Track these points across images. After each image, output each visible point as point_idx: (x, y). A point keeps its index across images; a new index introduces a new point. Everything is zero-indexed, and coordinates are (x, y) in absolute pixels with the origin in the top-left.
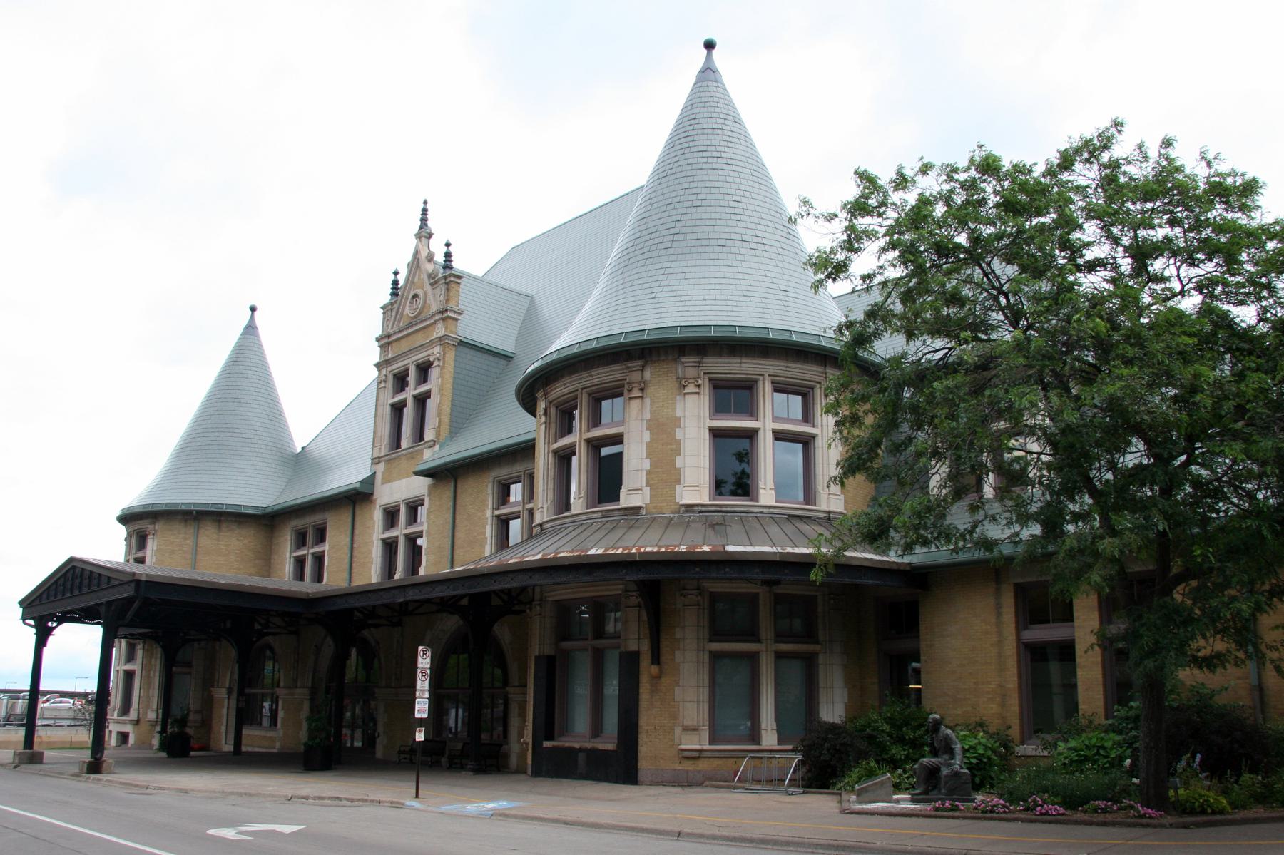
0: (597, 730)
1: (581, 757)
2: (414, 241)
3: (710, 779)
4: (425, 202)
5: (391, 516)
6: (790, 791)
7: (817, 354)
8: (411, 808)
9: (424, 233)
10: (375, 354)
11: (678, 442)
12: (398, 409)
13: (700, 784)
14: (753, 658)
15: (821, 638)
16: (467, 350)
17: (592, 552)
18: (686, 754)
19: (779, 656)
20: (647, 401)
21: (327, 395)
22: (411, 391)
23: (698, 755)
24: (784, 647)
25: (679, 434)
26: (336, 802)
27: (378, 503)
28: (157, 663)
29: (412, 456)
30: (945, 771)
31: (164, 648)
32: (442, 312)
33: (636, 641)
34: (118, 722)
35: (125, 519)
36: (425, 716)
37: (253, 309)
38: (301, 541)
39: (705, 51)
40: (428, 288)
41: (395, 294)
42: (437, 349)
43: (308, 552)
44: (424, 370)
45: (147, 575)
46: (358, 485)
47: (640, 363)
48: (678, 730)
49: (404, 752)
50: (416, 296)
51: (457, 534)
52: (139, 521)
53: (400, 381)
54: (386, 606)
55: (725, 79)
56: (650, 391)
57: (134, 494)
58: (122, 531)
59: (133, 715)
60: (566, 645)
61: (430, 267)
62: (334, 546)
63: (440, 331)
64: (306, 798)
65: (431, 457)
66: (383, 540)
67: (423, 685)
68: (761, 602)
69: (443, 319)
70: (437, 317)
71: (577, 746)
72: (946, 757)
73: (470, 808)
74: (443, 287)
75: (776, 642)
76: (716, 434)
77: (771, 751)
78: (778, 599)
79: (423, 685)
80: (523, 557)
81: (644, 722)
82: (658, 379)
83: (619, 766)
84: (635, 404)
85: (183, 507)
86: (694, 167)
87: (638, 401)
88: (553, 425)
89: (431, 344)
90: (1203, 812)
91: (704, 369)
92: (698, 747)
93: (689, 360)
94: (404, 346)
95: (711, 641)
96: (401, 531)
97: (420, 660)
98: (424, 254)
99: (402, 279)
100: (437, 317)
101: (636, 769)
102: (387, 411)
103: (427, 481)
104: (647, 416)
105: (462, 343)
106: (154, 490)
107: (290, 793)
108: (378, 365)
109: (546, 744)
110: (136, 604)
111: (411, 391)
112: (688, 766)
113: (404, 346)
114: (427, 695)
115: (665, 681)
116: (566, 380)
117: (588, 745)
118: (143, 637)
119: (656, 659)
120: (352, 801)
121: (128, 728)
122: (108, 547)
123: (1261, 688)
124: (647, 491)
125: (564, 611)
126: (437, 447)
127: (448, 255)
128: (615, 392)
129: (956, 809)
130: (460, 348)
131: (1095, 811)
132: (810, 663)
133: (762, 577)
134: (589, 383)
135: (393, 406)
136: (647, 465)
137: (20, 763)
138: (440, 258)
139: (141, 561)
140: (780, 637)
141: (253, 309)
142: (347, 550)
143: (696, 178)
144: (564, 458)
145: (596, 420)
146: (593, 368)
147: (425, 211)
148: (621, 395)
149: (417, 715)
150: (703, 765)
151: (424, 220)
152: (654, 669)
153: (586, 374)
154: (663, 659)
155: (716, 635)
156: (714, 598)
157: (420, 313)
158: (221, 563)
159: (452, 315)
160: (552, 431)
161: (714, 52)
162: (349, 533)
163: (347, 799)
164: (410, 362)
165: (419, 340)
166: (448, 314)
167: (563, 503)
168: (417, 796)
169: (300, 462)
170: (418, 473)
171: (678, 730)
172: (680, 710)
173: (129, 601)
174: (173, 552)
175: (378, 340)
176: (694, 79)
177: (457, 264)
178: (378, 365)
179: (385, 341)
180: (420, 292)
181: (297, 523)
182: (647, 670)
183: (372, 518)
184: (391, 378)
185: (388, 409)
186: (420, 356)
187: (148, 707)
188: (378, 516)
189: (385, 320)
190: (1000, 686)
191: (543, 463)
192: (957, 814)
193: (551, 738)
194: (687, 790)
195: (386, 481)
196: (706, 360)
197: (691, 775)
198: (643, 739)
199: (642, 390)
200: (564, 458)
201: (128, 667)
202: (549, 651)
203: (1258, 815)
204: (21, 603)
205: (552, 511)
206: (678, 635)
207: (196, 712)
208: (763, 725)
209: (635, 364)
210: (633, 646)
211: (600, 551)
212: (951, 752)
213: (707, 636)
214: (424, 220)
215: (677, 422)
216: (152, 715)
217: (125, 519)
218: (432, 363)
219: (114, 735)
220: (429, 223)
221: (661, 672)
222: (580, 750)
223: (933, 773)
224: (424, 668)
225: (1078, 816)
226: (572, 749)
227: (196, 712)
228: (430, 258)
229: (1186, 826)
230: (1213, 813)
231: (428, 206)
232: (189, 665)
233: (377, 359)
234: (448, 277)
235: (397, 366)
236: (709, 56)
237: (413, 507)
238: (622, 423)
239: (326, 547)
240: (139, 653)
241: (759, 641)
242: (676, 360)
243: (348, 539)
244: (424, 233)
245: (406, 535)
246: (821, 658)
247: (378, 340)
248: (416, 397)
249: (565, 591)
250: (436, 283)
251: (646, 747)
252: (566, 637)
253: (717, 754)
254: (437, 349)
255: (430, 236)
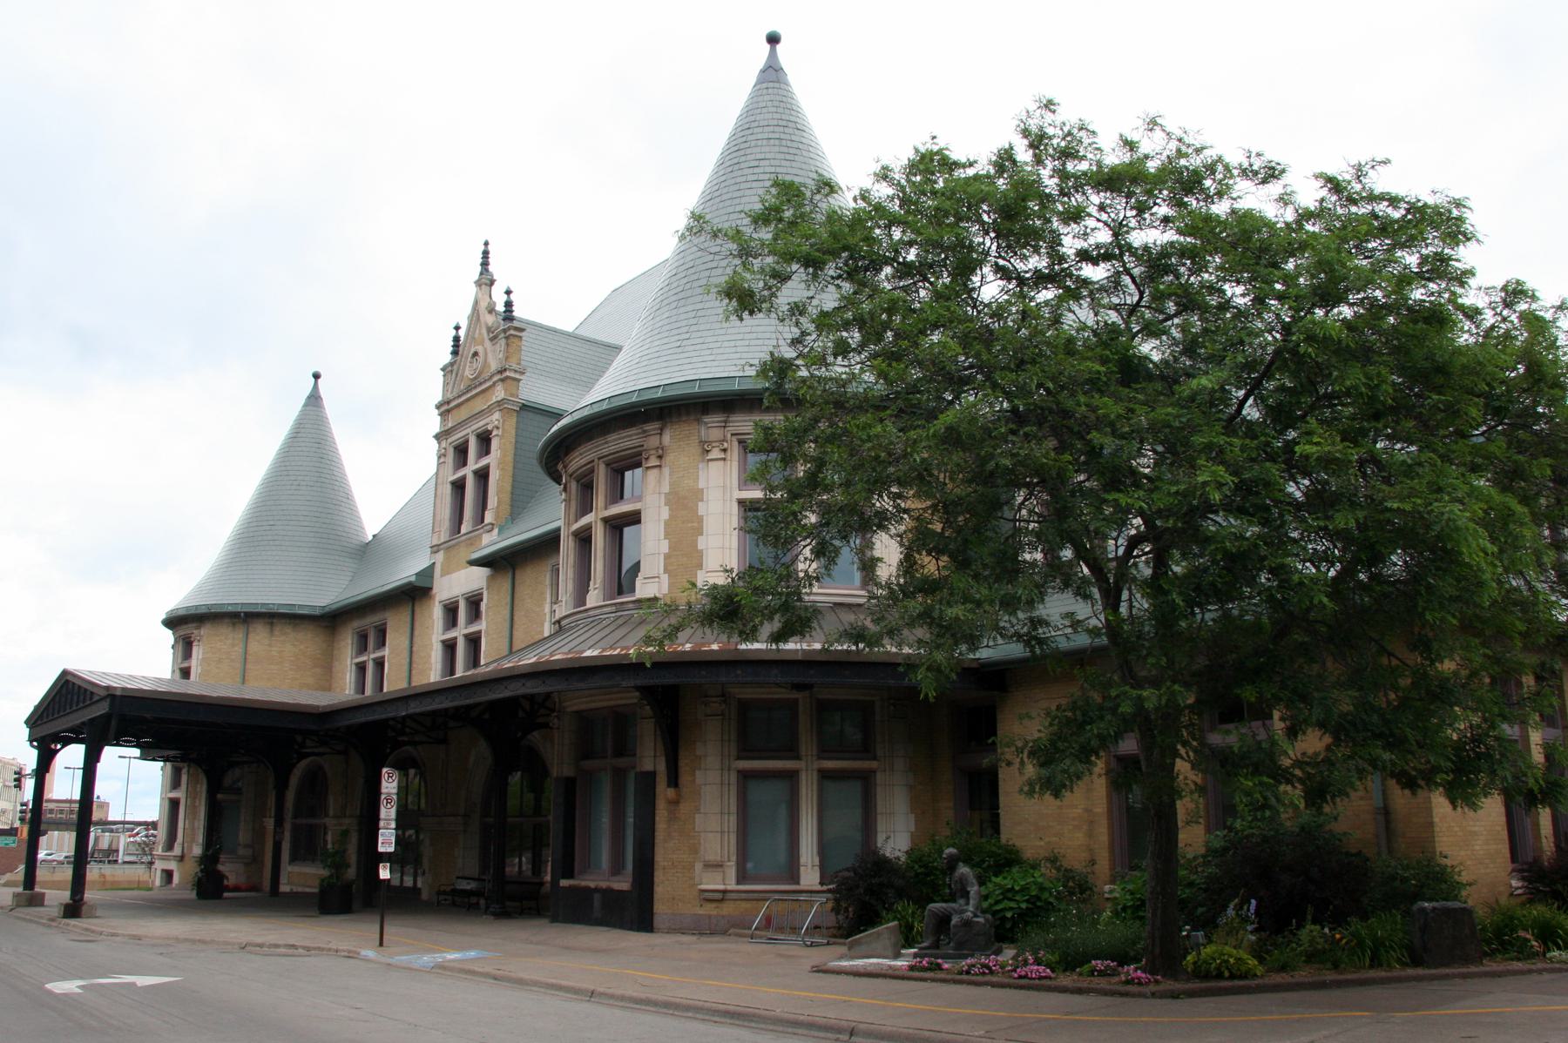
0: (617, 869)
1: (597, 897)
2: (473, 289)
3: (733, 926)
4: (486, 244)
5: (451, 611)
6: (808, 940)
7: (615, 419)
8: (367, 960)
9: (486, 280)
10: (434, 424)
11: (700, 520)
12: (459, 486)
13: (724, 933)
14: (792, 777)
15: (879, 753)
16: (531, 415)
17: (588, 653)
18: (710, 895)
19: (825, 775)
20: (666, 471)
21: (392, 476)
22: (473, 464)
23: (723, 896)
24: (829, 764)
25: (702, 509)
26: (291, 951)
27: (437, 599)
28: (203, 788)
29: (473, 541)
30: (955, 920)
31: (208, 774)
32: (500, 372)
33: (650, 758)
34: (163, 858)
35: (172, 622)
36: (391, 849)
37: (317, 376)
38: (362, 648)
39: (768, 47)
40: (488, 344)
41: (455, 353)
42: (497, 415)
43: (369, 658)
44: (485, 439)
45: (124, 689)
46: (413, 579)
47: (656, 425)
48: (699, 866)
49: (444, 893)
50: (476, 354)
51: (515, 633)
52: (184, 624)
53: (461, 452)
54: (393, 719)
55: (791, 78)
56: (669, 458)
57: (179, 592)
58: (168, 636)
59: (177, 851)
60: (588, 764)
61: (490, 319)
62: (393, 651)
63: (499, 393)
64: (261, 946)
65: (491, 542)
66: (443, 642)
67: (388, 813)
68: (801, 709)
69: (502, 380)
70: (496, 378)
71: (592, 885)
72: (962, 901)
73: (427, 959)
74: (503, 342)
75: (819, 758)
76: (741, 502)
77: (811, 892)
78: (823, 707)
79: (388, 813)
80: (551, 655)
81: (661, 857)
82: (675, 440)
83: (633, 911)
84: (653, 474)
85: (230, 609)
86: (743, 186)
87: (656, 471)
88: (573, 503)
89: (488, 411)
90: (1220, 976)
91: (731, 429)
92: (721, 887)
93: (714, 419)
94: (463, 413)
95: (739, 758)
96: (460, 632)
97: (384, 784)
98: (483, 305)
99: (462, 333)
100: (496, 378)
101: (652, 914)
102: (448, 489)
103: (483, 572)
104: (666, 489)
105: (526, 408)
106: (199, 589)
107: (244, 940)
108: (438, 437)
109: (564, 883)
110: (114, 723)
111: (473, 464)
112: (710, 909)
113: (463, 413)
114: (393, 825)
115: (684, 808)
116: (582, 449)
117: (604, 885)
118: (183, 759)
119: (674, 781)
120: (308, 949)
121: (172, 865)
122: (143, 660)
123: (1386, 812)
124: (665, 578)
125: (585, 722)
126: (496, 531)
127: (509, 304)
128: (634, 460)
129: (939, 967)
130: (524, 414)
131: (1092, 973)
132: (866, 780)
133: (632, 683)
134: (605, 452)
135: (454, 483)
136: (664, 547)
137: (18, 906)
138: (500, 308)
139: (186, 673)
140: (824, 752)
141: (317, 376)
142: (406, 654)
143: (744, 200)
144: (584, 539)
145: (617, 494)
146: (609, 432)
147: (486, 254)
148: (639, 465)
149: (381, 849)
150: (727, 909)
151: (485, 264)
152: (671, 792)
153: (601, 441)
154: (684, 779)
155: (746, 751)
156: (744, 707)
157: (480, 373)
158: (275, 676)
159: (512, 375)
160: (573, 509)
161: (778, 47)
162: (408, 630)
163: (304, 948)
164: (470, 433)
165: (479, 405)
166: (508, 373)
167: (580, 598)
168: (381, 944)
169: (367, 552)
170: (473, 563)
171: (699, 866)
172: (701, 839)
173: (106, 718)
174: (220, 661)
175: (438, 407)
176: (754, 81)
177: (518, 312)
178: (438, 437)
179: (445, 408)
180: (480, 349)
181: (357, 624)
182: (663, 792)
183: (431, 616)
184: (451, 451)
185: (449, 487)
186: (478, 425)
187: (193, 840)
188: (437, 613)
189: (446, 384)
190: (1087, 810)
191: (567, 547)
192: (940, 975)
193: (571, 875)
194: (704, 939)
195: (446, 571)
196: (733, 418)
197: (717, 922)
198: (659, 876)
199: (660, 457)
200: (584, 539)
201: (173, 795)
202: (568, 771)
203: (1301, 980)
204: (27, 722)
205: (571, 603)
206: (698, 753)
207: (246, 846)
208: (803, 860)
209: (652, 427)
210: (648, 766)
211: (596, 653)
212: (966, 895)
213: (734, 752)
214: (485, 264)
215: (698, 495)
216: (197, 850)
217: (172, 622)
218: (490, 432)
219: (159, 873)
220: (491, 268)
221: (679, 795)
222: (596, 890)
223: (943, 921)
224: (389, 794)
225: (1066, 980)
226: (587, 889)
227: (246, 846)
228: (491, 310)
229: (1175, 996)
230: (1232, 977)
231: (490, 248)
232: (238, 791)
233: (437, 429)
234: (508, 328)
235: (457, 437)
236: (773, 54)
237: (474, 602)
238: (640, 499)
239: (386, 652)
240: (184, 778)
241: (798, 758)
242: (698, 421)
243: (407, 642)
244: (486, 280)
245: (466, 636)
246: (879, 777)
247: (438, 407)
248: (476, 473)
249: (580, 699)
250: (495, 337)
251: (663, 887)
252: (587, 756)
253: (744, 896)
254: (497, 415)
255: (492, 282)
